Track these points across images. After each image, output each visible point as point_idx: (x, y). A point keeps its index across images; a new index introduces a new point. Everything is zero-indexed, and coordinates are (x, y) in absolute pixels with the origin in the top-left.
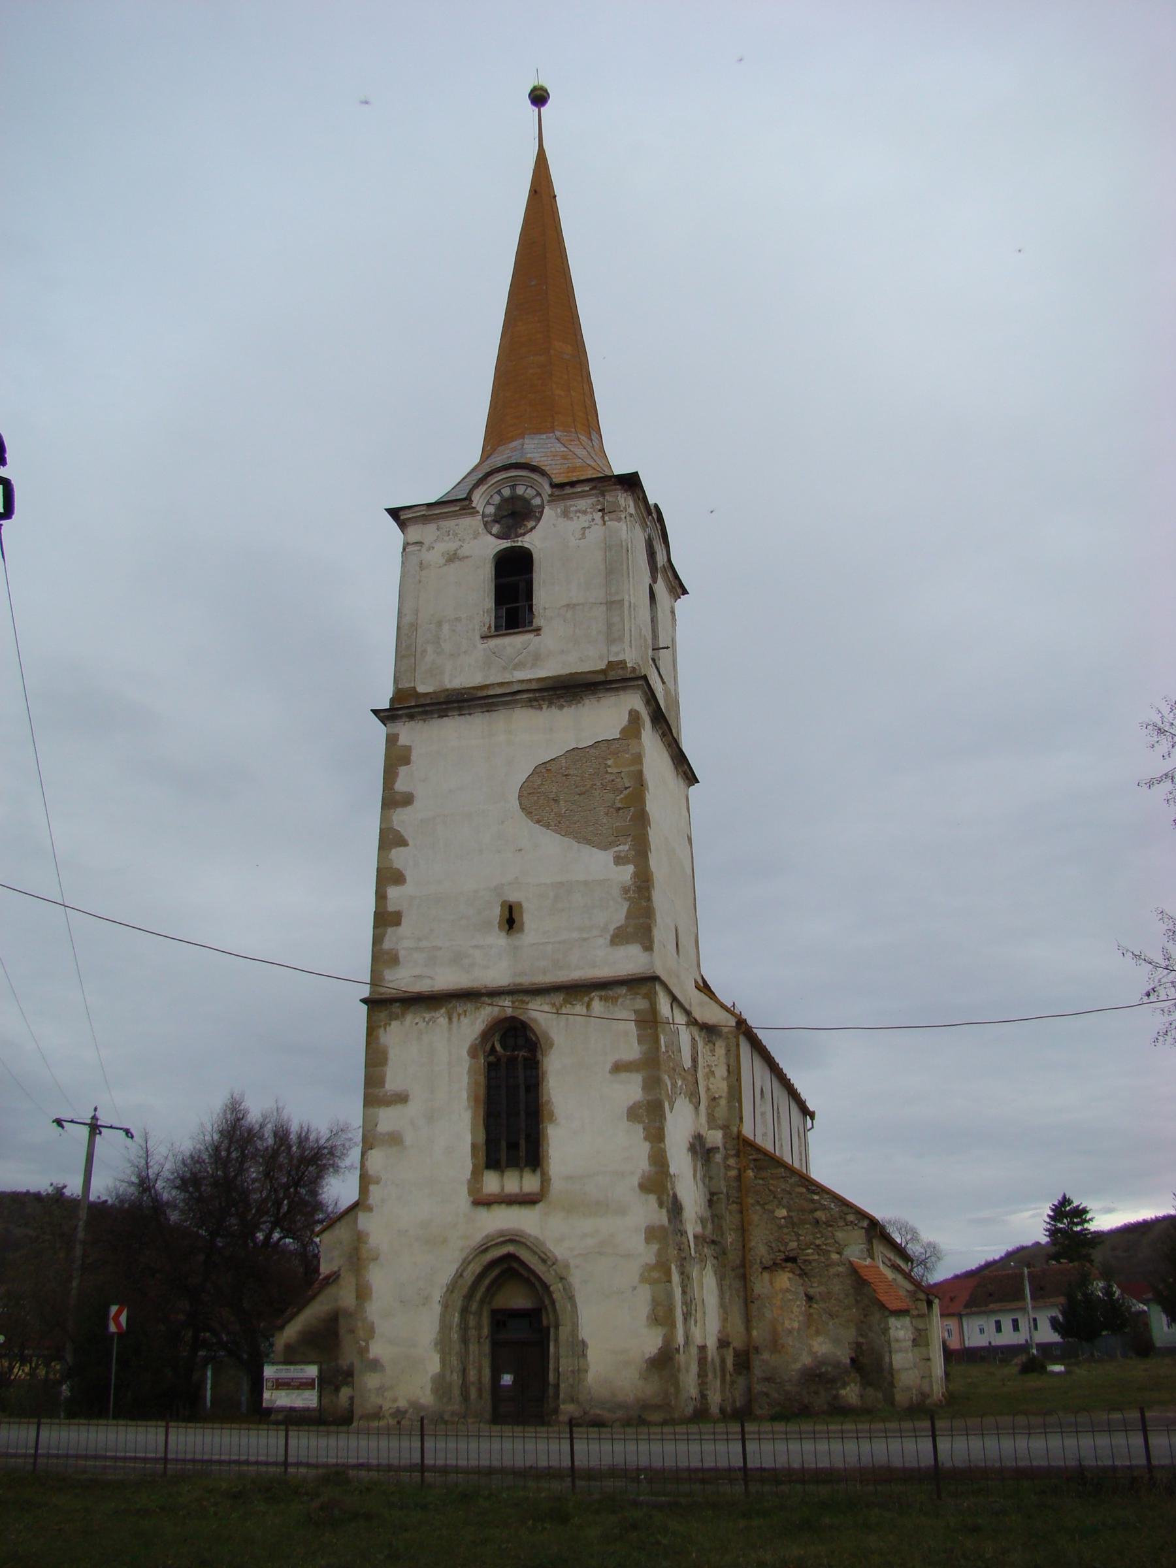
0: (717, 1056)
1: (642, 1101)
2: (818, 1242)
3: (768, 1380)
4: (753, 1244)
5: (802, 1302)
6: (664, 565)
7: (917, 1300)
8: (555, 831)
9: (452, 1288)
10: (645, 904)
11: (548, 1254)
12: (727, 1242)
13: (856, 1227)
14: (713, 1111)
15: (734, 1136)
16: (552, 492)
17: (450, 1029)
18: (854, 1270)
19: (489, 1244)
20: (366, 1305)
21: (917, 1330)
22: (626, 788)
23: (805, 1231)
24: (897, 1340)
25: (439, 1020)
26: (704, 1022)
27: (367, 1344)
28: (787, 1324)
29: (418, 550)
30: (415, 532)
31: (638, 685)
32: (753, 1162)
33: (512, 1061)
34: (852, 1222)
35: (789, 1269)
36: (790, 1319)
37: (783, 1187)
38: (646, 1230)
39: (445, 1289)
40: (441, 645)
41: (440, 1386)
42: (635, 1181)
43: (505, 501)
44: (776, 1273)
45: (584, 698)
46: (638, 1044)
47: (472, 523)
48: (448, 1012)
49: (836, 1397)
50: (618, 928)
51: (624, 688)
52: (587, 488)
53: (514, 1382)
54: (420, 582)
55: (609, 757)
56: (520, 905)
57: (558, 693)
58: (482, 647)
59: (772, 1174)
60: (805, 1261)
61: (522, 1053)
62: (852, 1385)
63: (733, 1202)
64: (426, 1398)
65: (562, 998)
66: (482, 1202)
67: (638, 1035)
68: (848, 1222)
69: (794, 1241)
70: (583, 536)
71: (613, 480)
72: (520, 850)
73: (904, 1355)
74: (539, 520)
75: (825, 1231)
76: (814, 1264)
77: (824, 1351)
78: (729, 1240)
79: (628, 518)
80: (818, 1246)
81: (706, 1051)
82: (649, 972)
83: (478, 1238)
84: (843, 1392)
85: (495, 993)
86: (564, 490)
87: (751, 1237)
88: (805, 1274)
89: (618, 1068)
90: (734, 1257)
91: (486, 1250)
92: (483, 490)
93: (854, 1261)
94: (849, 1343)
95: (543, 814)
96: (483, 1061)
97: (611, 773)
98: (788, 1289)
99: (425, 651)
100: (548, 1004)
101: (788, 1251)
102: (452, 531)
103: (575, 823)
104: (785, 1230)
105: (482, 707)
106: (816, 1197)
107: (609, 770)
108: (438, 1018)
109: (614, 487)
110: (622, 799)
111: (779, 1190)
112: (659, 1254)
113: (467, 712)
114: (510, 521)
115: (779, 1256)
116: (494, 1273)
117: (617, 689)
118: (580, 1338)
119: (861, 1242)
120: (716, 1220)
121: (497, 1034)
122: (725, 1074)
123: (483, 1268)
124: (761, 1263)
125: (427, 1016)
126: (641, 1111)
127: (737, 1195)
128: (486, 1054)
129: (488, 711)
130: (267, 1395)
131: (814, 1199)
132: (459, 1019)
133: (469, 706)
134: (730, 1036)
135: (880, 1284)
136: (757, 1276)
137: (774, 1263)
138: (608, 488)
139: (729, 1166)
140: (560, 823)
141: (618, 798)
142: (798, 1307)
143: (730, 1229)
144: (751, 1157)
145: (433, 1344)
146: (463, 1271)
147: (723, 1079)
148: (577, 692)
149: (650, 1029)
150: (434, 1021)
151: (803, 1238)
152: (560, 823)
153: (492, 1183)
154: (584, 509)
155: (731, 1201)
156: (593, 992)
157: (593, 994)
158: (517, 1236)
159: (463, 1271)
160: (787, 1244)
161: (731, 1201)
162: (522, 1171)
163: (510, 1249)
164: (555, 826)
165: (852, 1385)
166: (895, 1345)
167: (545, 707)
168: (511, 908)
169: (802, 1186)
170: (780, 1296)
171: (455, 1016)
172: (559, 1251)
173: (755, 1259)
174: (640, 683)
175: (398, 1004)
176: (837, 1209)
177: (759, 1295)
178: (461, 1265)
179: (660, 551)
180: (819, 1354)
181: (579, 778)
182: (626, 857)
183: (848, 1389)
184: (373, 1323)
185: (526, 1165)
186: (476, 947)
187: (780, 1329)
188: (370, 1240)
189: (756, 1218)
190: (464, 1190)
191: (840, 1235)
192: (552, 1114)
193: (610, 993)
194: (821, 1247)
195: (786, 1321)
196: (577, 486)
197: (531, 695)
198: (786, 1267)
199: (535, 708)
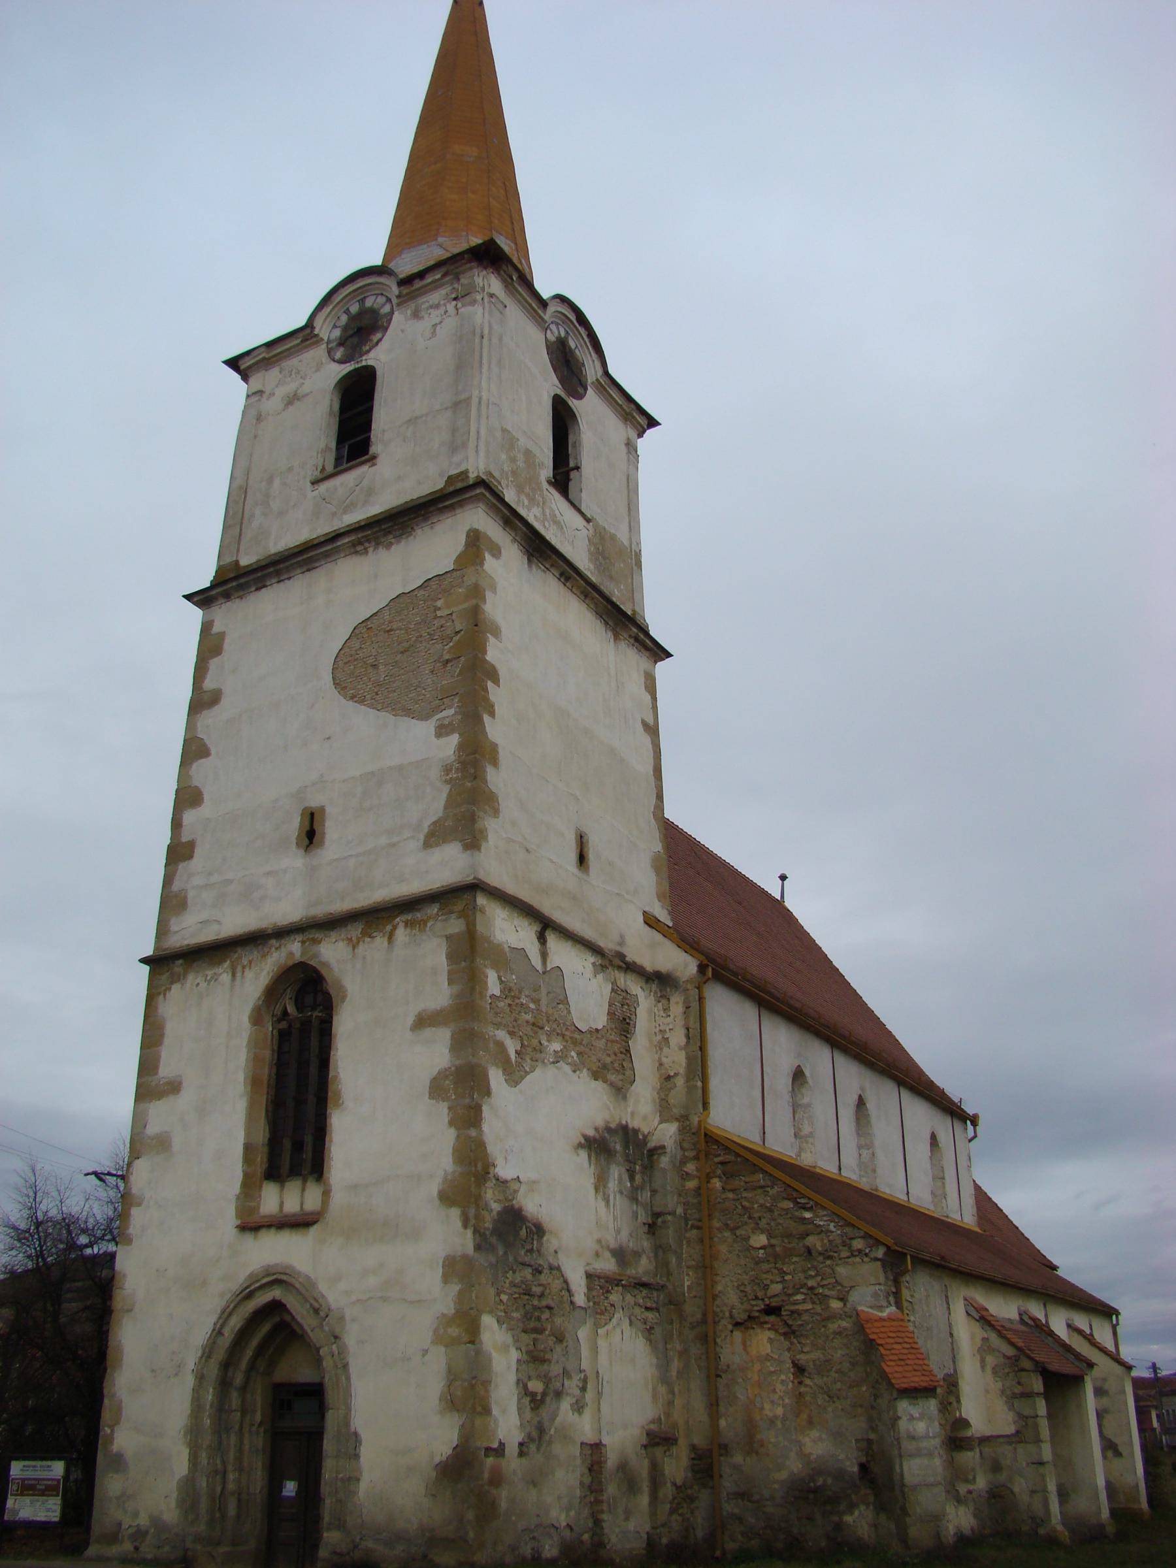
0: (672, 1017)
1: (450, 1068)
2: (811, 1283)
3: (742, 1495)
4: (719, 1288)
5: (788, 1376)
6: (597, 380)
7: (1023, 1370)
8: (371, 706)
9: (208, 1353)
10: (469, 784)
11: (320, 1300)
12: (683, 1285)
13: (866, 1259)
14: (667, 1095)
15: (693, 1131)
16: (400, 292)
17: (232, 987)
18: (860, 1325)
19: (253, 1287)
20: (116, 1375)
21: (1021, 1416)
22: (457, 633)
23: (792, 1267)
24: (912, 1438)
25: (221, 977)
26: (656, 970)
27: (112, 1431)
28: (768, 1410)
29: (257, 401)
30: (257, 381)
31: (477, 495)
32: (720, 1166)
33: (306, 1024)
34: (860, 1251)
35: (769, 1326)
36: (772, 1402)
37: (761, 1201)
38: (444, 1262)
39: (199, 1354)
40: (269, 505)
41: (188, 1492)
42: (434, 1188)
43: (353, 318)
44: (752, 1331)
45: (415, 528)
46: (449, 984)
47: (319, 353)
48: (233, 965)
49: (838, 1527)
50: (434, 823)
51: (461, 504)
52: (438, 276)
53: (298, 1492)
54: (255, 437)
55: (440, 596)
56: (322, 809)
57: (383, 527)
58: (311, 494)
59: (746, 1183)
60: (793, 1312)
61: (316, 1014)
62: (862, 1508)
63: (693, 1227)
64: (170, 1513)
65: (360, 930)
66: (251, 1226)
67: (450, 973)
68: (854, 1251)
69: (777, 1283)
70: (434, 334)
71: (466, 256)
72: (328, 738)
73: (926, 1462)
74: (386, 329)
75: (821, 1266)
76: (805, 1317)
77: (820, 1452)
78: (687, 1283)
79: (486, 300)
80: (812, 1288)
81: (658, 1010)
82: (468, 879)
83: (240, 1278)
84: (848, 1519)
85: (282, 933)
86: (413, 286)
87: (718, 1278)
88: (794, 1332)
89: (422, 1022)
90: (692, 1309)
91: (250, 1296)
92: (327, 313)
93: (863, 1311)
94: (856, 1440)
95: (359, 687)
96: (271, 1029)
97: (441, 617)
98: (768, 1354)
99: (253, 515)
100: (343, 940)
101: (770, 1298)
102: (294, 370)
103: (395, 691)
104: (765, 1266)
105: (301, 566)
106: (808, 1215)
107: (439, 613)
108: (221, 974)
109: (468, 265)
110: (451, 647)
111: (756, 1206)
112: (461, 1297)
113: (286, 576)
114: (355, 340)
115: (756, 1305)
116: (265, 1328)
117: (452, 507)
118: (353, 1430)
119: (873, 1282)
120: (660, 1253)
121: (289, 991)
122: (683, 1040)
123: (245, 1321)
124: (731, 1316)
125: (210, 973)
126: (447, 1082)
127: (697, 1216)
128: (275, 1019)
129: (308, 570)
130: (10, 1503)
131: (805, 1218)
132: (243, 972)
133: (287, 567)
134: (689, 987)
135: (896, 1346)
136: (726, 1336)
137: (749, 1317)
138: (461, 269)
139: (687, 1174)
140: (377, 694)
141: (446, 647)
142: (784, 1381)
143: (688, 1267)
144: (717, 1160)
145: (182, 1433)
146: (222, 1326)
147: (681, 1049)
148: (405, 521)
149: (465, 961)
150: (215, 978)
151: (790, 1277)
152: (377, 694)
153: (271, 1200)
154: (437, 302)
155: (689, 1226)
156: (397, 916)
157: (398, 919)
158: (286, 1274)
159: (222, 1326)
160: (766, 1288)
161: (689, 1226)
162: (305, 1181)
163: (276, 1293)
164: (372, 699)
165: (862, 1508)
166: (907, 1445)
167: (370, 550)
168: (312, 814)
169: (789, 1200)
170: (757, 1367)
171: (239, 968)
172: (333, 1296)
173: (721, 1311)
174: (478, 491)
175: (180, 961)
176: (839, 1232)
177: (728, 1366)
178: (220, 1318)
179: (591, 362)
180: (813, 1457)
181: (403, 632)
182: (451, 724)
183: (856, 1513)
184: (121, 1401)
185: (311, 1173)
186: (268, 874)
187: (757, 1417)
188: (127, 1283)
189: (723, 1249)
190: (230, 1211)
191: (841, 1270)
192: (338, 1095)
193: (419, 915)
194: (816, 1291)
195: (765, 1405)
196: (427, 276)
197: (353, 538)
198: (766, 1323)
199: (361, 554)
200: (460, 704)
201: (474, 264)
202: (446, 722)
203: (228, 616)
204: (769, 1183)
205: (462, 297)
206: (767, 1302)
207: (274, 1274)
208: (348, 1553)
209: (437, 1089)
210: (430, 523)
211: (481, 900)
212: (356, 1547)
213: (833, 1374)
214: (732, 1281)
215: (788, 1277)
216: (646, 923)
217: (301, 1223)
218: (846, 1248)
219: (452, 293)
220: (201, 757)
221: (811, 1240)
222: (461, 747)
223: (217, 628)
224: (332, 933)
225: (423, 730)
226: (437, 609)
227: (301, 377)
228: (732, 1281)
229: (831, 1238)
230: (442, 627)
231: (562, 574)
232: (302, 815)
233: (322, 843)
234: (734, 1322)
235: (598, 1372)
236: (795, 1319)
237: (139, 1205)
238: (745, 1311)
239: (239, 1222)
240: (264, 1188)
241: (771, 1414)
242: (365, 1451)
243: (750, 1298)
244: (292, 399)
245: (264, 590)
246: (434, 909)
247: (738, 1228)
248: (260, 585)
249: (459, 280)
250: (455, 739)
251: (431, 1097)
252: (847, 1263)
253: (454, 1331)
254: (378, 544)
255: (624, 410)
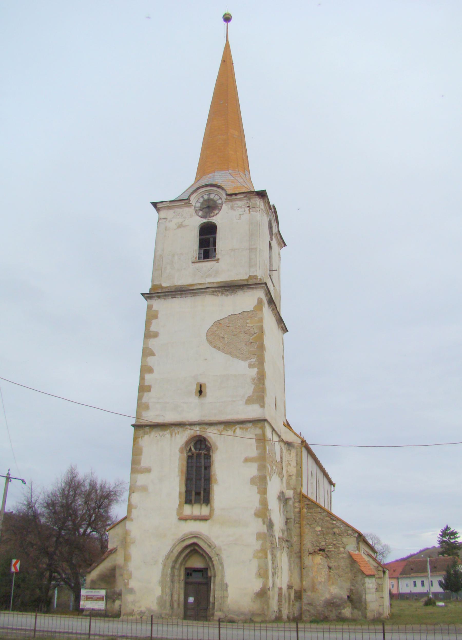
2: (334, 542)
3: (310, 604)
4: (305, 542)
5: (326, 569)
6: (276, 233)
8: (222, 352)
9: (167, 558)
13: (352, 537)
18: (350, 556)
22: (255, 333)
23: (329, 537)
24: (369, 588)
25: (166, 435)
27: (128, 581)
30: (164, 213)
31: (262, 287)
32: (306, 505)
33: (199, 455)
34: (350, 534)
37: (320, 517)
39: (164, 558)
42: (253, 512)
43: (205, 201)
49: (340, 613)
50: (249, 397)
51: (256, 288)
52: (243, 197)
57: (226, 289)
60: (328, 551)
62: (348, 608)
63: (297, 523)
66: (183, 519)
67: (257, 446)
71: (254, 193)
76: (332, 553)
78: (294, 540)
79: (261, 211)
80: (335, 544)
84: (343, 611)
88: (328, 557)
90: (296, 548)
91: (184, 540)
94: (347, 589)
97: (249, 326)
100: (216, 430)
101: (321, 546)
104: (320, 537)
106: (334, 522)
108: (166, 434)
109: (255, 196)
113: (184, 296)
114: (207, 210)
117: (253, 288)
118: (225, 582)
120: (289, 531)
122: (295, 464)
124: (308, 551)
126: (256, 480)
129: (194, 296)
131: (333, 523)
132: (175, 435)
133: (185, 293)
136: (306, 557)
137: (314, 551)
138: (252, 197)
139: (295, 506)
140: (224, 348)
143: (295, 535)
144: (305, 503)
146: (173, 549)
153: (188, 510)
154: (241, 206)
155: (295, 523)
156: (237, 425)
157: (237, 426)
158: (198, 534)
159: (173, 549)
160: (320, 543)
161: (295, 523)
162: (201, 505)
164: (222, 349)
165: (348, 608)
166: (367, 591)
167: (220, 295)
168: (201, 386)
171: (174, 434)
172: (217, 542)
175: (148, 428)
179: (275, 226)
180: (333, 593)
181: (234, 328)
183: (346, 609)
184: (131, 572)
185: (204, 503)
189: (307, 530)
190: (175, 513)
192: (216, 480)
194: (336, 545)
197: (213, 289)
198: (320, 553)
200: (257, 358)
201: (257, 196)
202: (252, 363)
203: (157, 304)
204: (322, 512)
205: (252, 208)
206: (320, 547)
207: (194, 534)
208: (224, 618)
209: (253, 481)
210: (243, 291)
211: (267, 425)
212: (226, 616)
213: (340, 570)
214: (309, 541)
215: (327, 540)
216: (283, 425)
217: (204, 519)
218: (346, 533)
219: (247, 204)
220: (152, 356)
221: (335, 530)
222: (258, 373)
223: (155, 308)
224: (211, 427)
225: (245, 364)
226: (247, 323)
227: (184, 218)
228: (309, 541)
229: (341, 530)
230: (249, 330)
231: (273, 309)
232: (197, 385)
233: (205, 396)
234: (309, 553)
235: (281, 567)
236: (329, 553)
237: (136, 508)
238: (313, 550)
239: (178, 517)
240: (184, 507)
241: (320, 581)
242: (229, 589)
243: (315, 545)
244: (180, 226)
245: (174, 299)
246: (250, 425)
247: (312, 524)
248: (173, 297)
249: (250, 200)
250: (256, 370)
251: (251, 484)
252: (346, 537)
253: (260, 554)
254: (222, 294)
255: (279, 242)
